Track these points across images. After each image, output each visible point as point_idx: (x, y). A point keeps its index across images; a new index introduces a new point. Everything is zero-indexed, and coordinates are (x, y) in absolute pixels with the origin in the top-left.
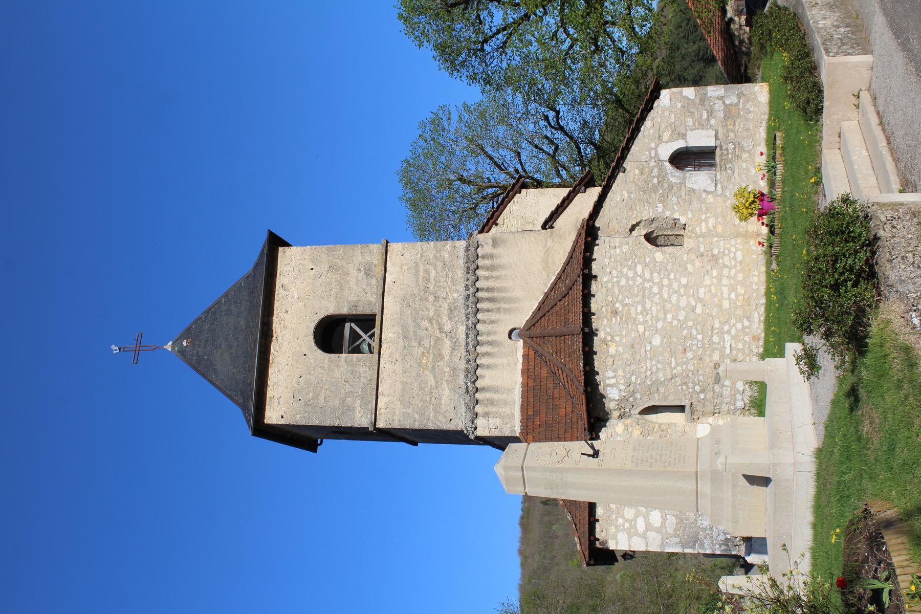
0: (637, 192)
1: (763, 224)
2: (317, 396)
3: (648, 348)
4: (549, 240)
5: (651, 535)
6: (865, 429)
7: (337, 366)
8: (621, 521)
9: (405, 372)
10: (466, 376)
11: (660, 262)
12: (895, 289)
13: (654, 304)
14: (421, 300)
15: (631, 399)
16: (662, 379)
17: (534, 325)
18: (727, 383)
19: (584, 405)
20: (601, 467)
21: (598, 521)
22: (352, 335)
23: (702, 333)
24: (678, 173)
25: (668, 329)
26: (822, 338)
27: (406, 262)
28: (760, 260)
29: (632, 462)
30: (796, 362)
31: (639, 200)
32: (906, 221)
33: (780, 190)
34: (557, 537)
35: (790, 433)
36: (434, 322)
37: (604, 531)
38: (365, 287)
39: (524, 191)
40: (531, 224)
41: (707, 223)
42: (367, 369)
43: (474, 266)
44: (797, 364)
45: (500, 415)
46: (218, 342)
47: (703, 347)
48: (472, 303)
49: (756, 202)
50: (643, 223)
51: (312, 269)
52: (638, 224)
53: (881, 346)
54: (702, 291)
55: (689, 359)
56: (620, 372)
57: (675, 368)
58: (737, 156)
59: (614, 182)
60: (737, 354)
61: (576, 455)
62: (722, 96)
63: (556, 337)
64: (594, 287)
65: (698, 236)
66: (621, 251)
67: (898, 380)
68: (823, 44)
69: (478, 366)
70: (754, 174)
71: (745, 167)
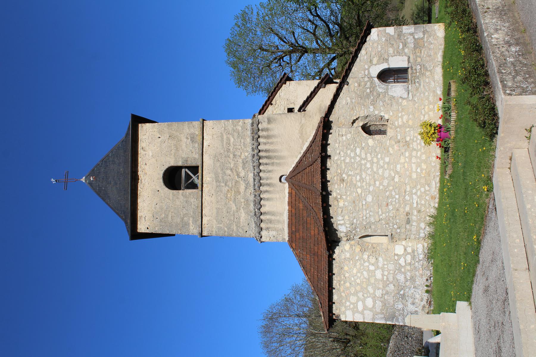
0: (356, 98)
2: (167, 216)
3: (364, 203)
4: (303, 119)
7: (178, 198)
8: (348, 304)
9: (218, 202)
10: (255, 205)
11: (372, 146)
14: (225, 157)
15: (354, 232)
18: (414, 224)
23: (399, 194)
25: (377, 191)
27: (215, 133)
36: (234, 171)
37: (338, 309)
38: (191, 148)
39: (288, 83)
41: (402, 119)
42: (195, 200)
43: (256, 136)
45: (276, 229)
46: (109, 180)
48: (256, 160)
49: (435, 133)
51: (159, 137)
52: (357, 119)
54: (399, 166)
59: (341, 91)
60: (421, 207)
62: (413, 33)
64: (329, 163)
66: (346, 138)
69: (261, 199)
70: (433, 86)
71: (428, 81)
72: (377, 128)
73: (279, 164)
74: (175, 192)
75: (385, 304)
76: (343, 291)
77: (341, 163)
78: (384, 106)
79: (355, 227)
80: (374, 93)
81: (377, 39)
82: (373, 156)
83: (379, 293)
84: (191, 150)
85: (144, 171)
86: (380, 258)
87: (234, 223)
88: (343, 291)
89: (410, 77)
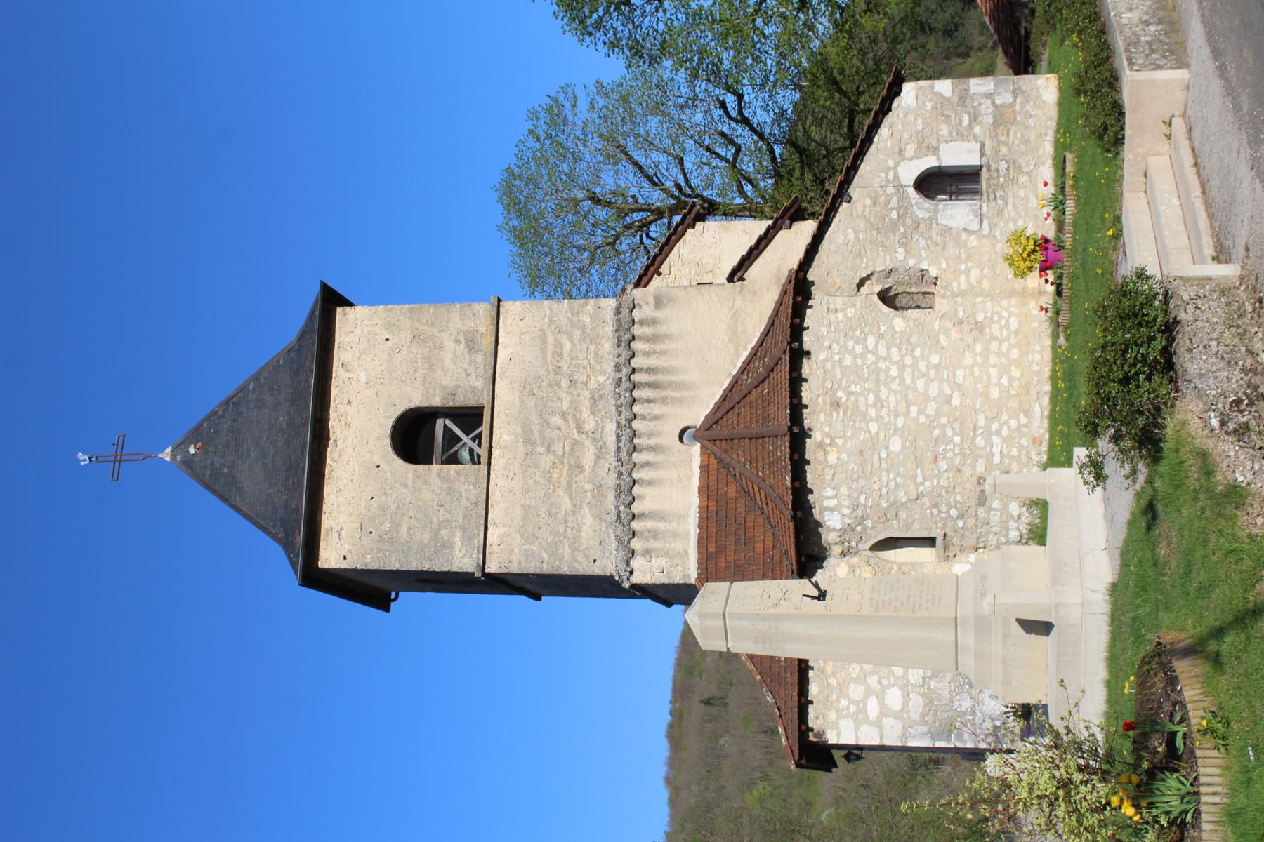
0: (868, 231)
1: (1047, 281)
2: (396, 526)
3: (884, 455)
4: (738, 298)
5: (888, 722)
6: (1162, 552)
7: (427, 483)
8: (844, 703)
9: (527, 491)
10: (618, 497)
11: (901, 332)
12: (1193, 385)
13: (892, 393)
14: (550, 385)
15: (859, 529)
16: (904, 500)
17: (717, 422)
19: (792, 536)
20: (829, 613)
21: (811, 702)
22: (447, 437)
23: (961, 434)
24: (927, 204)
26: (1110, 442)
28: (1044, 330)
29: (871, 605)
30: (1078, 471)
31: (871, 242)
32: (1213, 301)
33: (1070, 235)
34: (727, 756)
35: (1078, 565)
37: (821, 718)
38: (466, 366)
39: (699, 225)
40: (710, 274)
41: (968, 277)
42: (471, 487)
43: (627, 336)
44: (1080, 473)
45: (667, 553)
46: (245, 447)
47: (962, 453)
48: (626, 390)
49: (1037, 251)
50: (876, 276)
51: (387, 340)
52: (868, 277)
53: (1177, 451)
54: (960, 373)
55: (942, 470)
56: (844, 490)
57: (922, 484)
58: (1012, 180)
59: (834, 216)
60: (1010, 465)
61: (796, 597)
62: (991, 94)
63: (750, 439)
64: (807, 368)
65: (954, 295)
66: (845, 315)
67: (1195, 490)
68: (1127, 50)
69: (634, 482)
71: (1023, 195)
72: (911, 303)
73: (678, 401)
74: (420, 468)
75: (931, 702)
76: (833, 674)
77: (833, 367)
78: (929, 248)
79: (863, 516)
80: (907, 220)
81: (915, 105)
82: (904, 351)
84: (466, 370)
85: (343, 418)
87: (566, 539)
88: (833, 672)
89: (984, 187)
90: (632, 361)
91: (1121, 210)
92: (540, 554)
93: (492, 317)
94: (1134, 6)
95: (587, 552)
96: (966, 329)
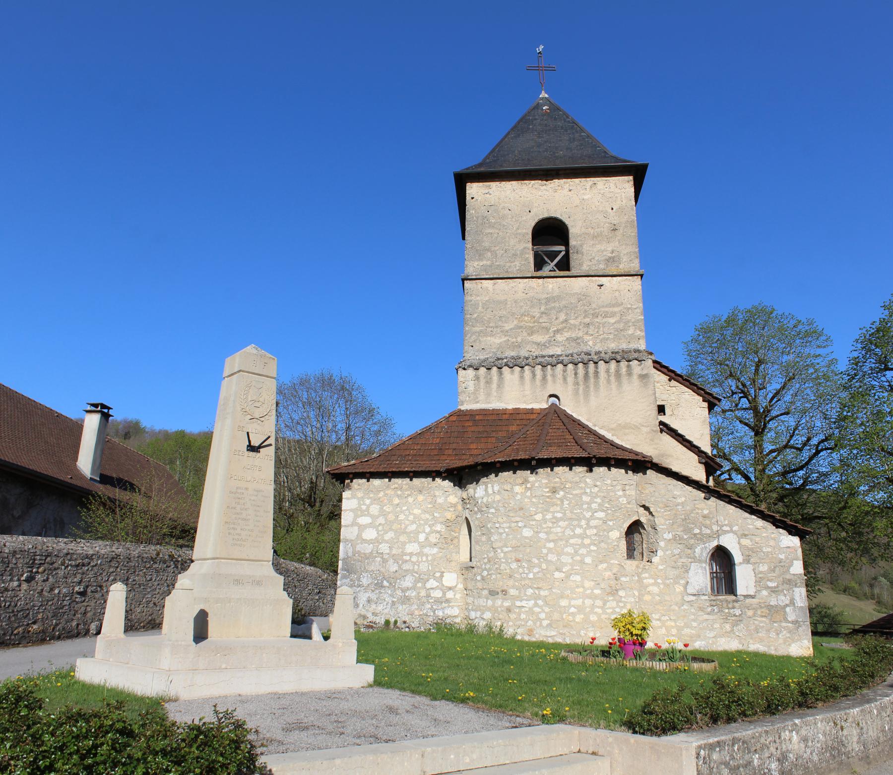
0: (683, 512)
2: (492, 226)
3: (520, 524)
7: (520, 241)
8: (368, 502)
9: (515, 302)
10: (513, 358)
13: (563, 530)
14: (585, 311)
15: (476, 509)
21: (368, 481)
23: (535, 578)
25: (539, 544)
31: (675, 514)
38: (596, 258)
39: (706, 405)
40: (671, 413)
41: (653, 584)
42: (518, 268)
43: (619, 358)
45: (477, 391)
48: (582, 359)
49: (632, 636)
51: (612, 209)
52: (651, 513)
54: (578, 578)
56: (498, 498)
57: (502, 551)
59: (694, 488)
60: (515, 612)
62: (794, 604)
64: (580, 470)
66: (620, 496)
69: (522, 367)
71: (715, 626)
73: (576, 392)
74: (529, 237)
75: (367, 558)
76: (386, 495)
79: (482, 511)
80: (693, 541)
81: (782, 546)
83: (384, 548)
86: (437, 550)
89: (720, 597)
90: (602, 362)
91: (570, 724)
92: (476, 313)
93: (630, 272)
94: (810, 744)
95: (478, 341)
96: (612, 583)
